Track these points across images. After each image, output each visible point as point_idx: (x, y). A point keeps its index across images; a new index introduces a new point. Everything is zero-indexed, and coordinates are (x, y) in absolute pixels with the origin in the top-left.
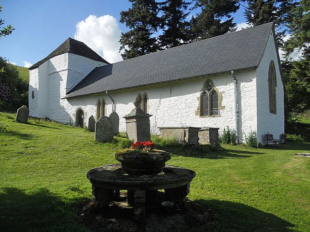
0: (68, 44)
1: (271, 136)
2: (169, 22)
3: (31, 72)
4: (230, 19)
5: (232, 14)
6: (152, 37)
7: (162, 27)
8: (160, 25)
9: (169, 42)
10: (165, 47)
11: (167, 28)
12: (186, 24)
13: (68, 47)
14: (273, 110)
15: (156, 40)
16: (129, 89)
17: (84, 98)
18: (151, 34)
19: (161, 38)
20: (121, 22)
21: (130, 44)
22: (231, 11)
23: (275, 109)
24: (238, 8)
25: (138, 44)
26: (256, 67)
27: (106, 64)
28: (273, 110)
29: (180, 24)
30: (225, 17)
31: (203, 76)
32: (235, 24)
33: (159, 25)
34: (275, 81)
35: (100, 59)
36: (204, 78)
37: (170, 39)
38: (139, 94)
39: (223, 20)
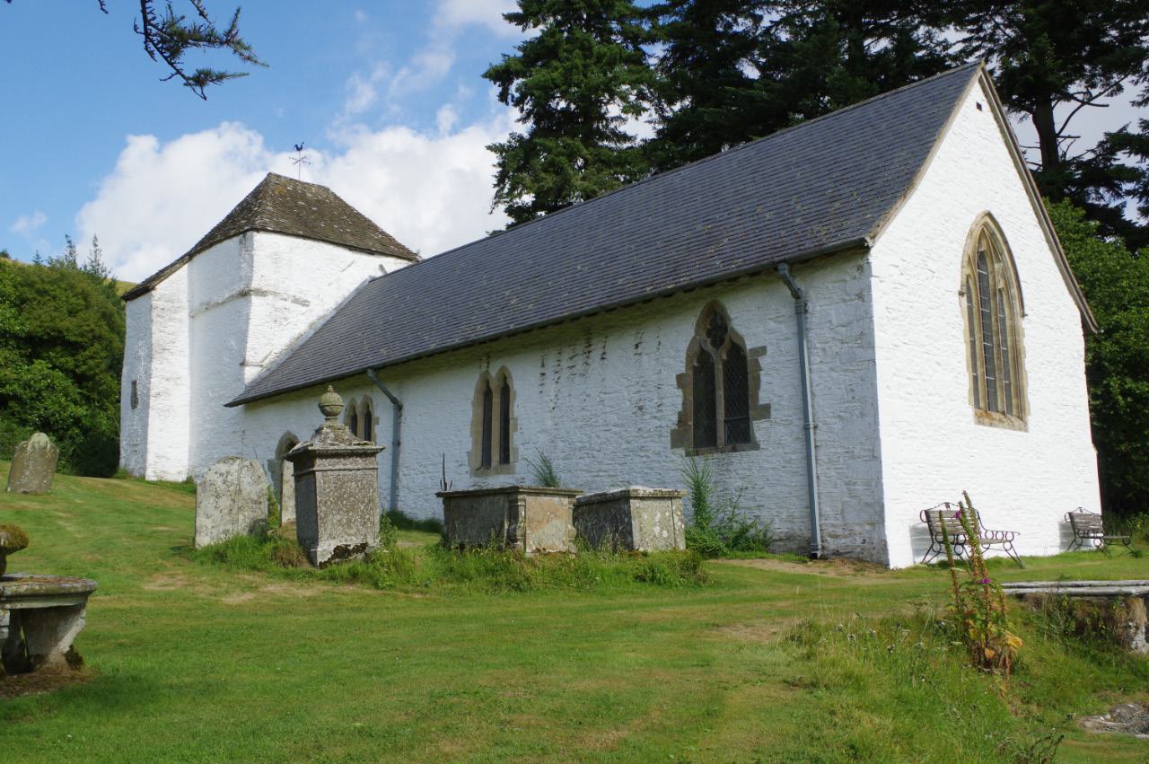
17: (299, 398)
31: (688, 289)
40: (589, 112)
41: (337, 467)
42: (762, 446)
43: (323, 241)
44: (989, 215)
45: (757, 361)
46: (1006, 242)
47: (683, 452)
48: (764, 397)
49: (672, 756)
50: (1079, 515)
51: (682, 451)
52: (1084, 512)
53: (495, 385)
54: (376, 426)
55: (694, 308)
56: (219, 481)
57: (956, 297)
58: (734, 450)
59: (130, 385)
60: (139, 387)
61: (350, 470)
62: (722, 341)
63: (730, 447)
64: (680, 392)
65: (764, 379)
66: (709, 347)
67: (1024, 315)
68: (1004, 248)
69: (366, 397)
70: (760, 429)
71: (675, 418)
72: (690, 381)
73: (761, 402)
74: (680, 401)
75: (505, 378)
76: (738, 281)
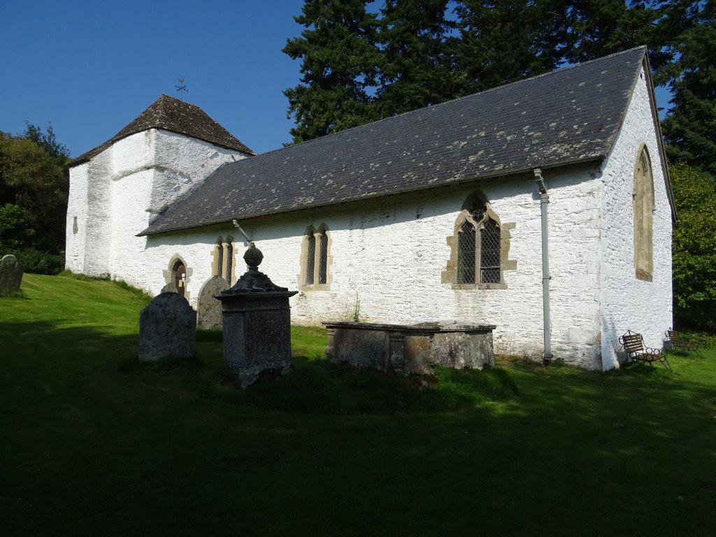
23: (650, 267)
40: (343, 77)
42: (509, 287)
45: (508, 232)
47: (450, 287)
48: (511, 255)
58: (488, 288)
60: (78, 221)
61: (271, 310)
63: (485, 285)
64: (449, 248)
65: (512, 244)
66: (472, 221)
69: (220, 237)
70: (507, 275)
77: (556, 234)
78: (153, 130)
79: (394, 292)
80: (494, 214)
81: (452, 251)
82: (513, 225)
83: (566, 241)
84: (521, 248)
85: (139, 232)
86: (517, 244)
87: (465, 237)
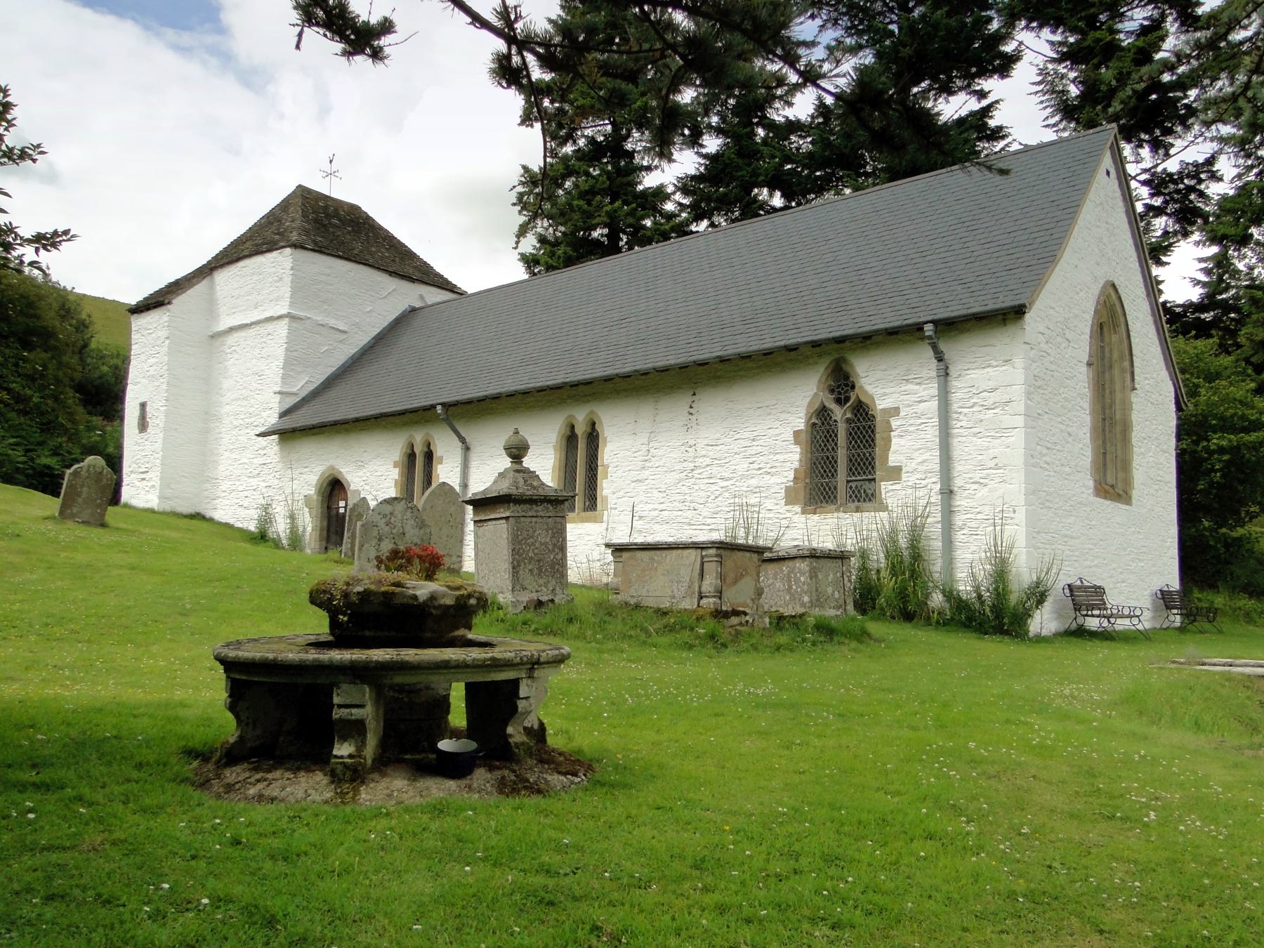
0: (299, 201)
1: (1099, 591)
2: (723, 119)
3: (140, 324)
4: (985, 103)
5: (991, 85)
6: (649, 181)
7: (694, 141)
8: (687, 132)
9: (724, 204)
10: (705, 223)
11: (712, 144)
12: (794, 126)
13: (295, 224)
14: (1112, 481)
15: (667, 197)
16: (513, 400)
17: (347, 431)
18: (649, 169)
19: (686, 185)
20: (523, 123)
21: (559, 216)
22: (984, 73)
23: (1128, 482)
24: (1014, 58)
25: (582, 213)
26: (1017, 312)
27: (447, 296)
28: (1112, 481)
29: (770, 125)
30: (961, 97)
31: (815, 344)
32: (1000, 128)
33: (683, 135)
34: (1127, 364)
35: (424, 275)
36: (820, 356)
37: (723, 191)
38: (569, 416)
39: (952, 108)
41: (530, 514)
43: (378, 269)
44: (1114, 286)
45: (888, 422)
46: (1125, 315)
48: (893, 460)
49: (31, 816)
50: (1079, 588)
51: (798, 509)
52: (1086, 583)
53: (581, 430)
54: (439, 467)
55: (816, 363)
56: (382, 523)
57: (1084, 369)
59: (138, 408)
60: (148, 409)
62: (847, 399)
63: (852, 506)
67: (1134, 389)
68: (1122, 319)
71: (792, 477)
72: (803, 437)
73: (890, 464)
74: (797, 457)
75: (594, 424)
76: (869, 341)
77: (959, 424)
78: (288, 251)
79: (709, 521)
80: (866, 392)
81: (801, 453)
82: (896, 411)
83: (975, 435)
84: (908, 447)
85: (262, 429)
86: (902, 442)
87: (819, 433)
